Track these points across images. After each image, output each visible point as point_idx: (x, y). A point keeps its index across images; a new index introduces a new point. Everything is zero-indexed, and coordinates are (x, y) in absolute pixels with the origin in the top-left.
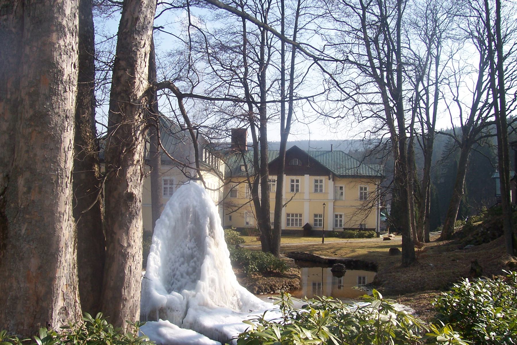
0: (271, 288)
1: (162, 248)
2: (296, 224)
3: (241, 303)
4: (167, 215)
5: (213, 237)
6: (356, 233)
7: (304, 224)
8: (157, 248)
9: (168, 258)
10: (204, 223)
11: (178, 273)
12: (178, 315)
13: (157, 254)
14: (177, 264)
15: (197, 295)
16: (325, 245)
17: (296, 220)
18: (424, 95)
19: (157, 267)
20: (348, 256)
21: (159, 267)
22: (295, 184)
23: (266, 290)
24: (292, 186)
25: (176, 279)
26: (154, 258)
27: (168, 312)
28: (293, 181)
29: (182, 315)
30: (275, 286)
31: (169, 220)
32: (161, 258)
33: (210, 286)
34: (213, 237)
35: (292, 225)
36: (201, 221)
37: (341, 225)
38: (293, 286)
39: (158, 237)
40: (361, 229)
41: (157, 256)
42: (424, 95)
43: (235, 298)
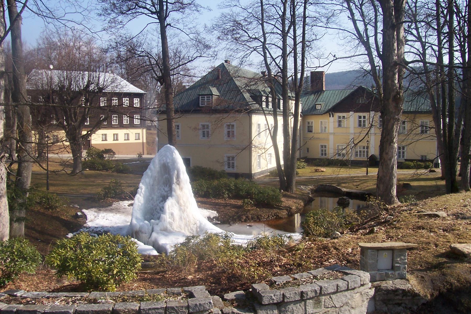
0: (258, 218)
1: (145, 191)
2: (364, 155)
3: (198, 230)
4: (150, 169)
5: (179, 184)
6: (412, 164)
7: (370, 155)
8: (141, 192)
9: (151, 198)
10: (173, 175)
11: (158, 208)
12: (144, 236)
13: (140, 196)
14: (158, 202)
15: (159, 224)
16: (368, 177)
17: (364, 152)
18: (445, 48)
19: (140, 204)
20: (370, 187)
21: (142, 204)
22: (362, 119)
23: (252, 218)
24: (360, 122)
25: (157, 212)
26: (138, 198)
27: (140, 234)
28: (360, 117)
29: (148, 237)
30: (261, 216)
31: (151, 172)
32: (144, 197)
33: (169, 218)
34: (179, 184)
35: (360, 155)
36: (171, 173)
37: (403, 157)
38: (278, 216)
39: (143, 184)
40: (421, 161)
41: (140, 197)
42: (445, 48)
43: (195, 226)
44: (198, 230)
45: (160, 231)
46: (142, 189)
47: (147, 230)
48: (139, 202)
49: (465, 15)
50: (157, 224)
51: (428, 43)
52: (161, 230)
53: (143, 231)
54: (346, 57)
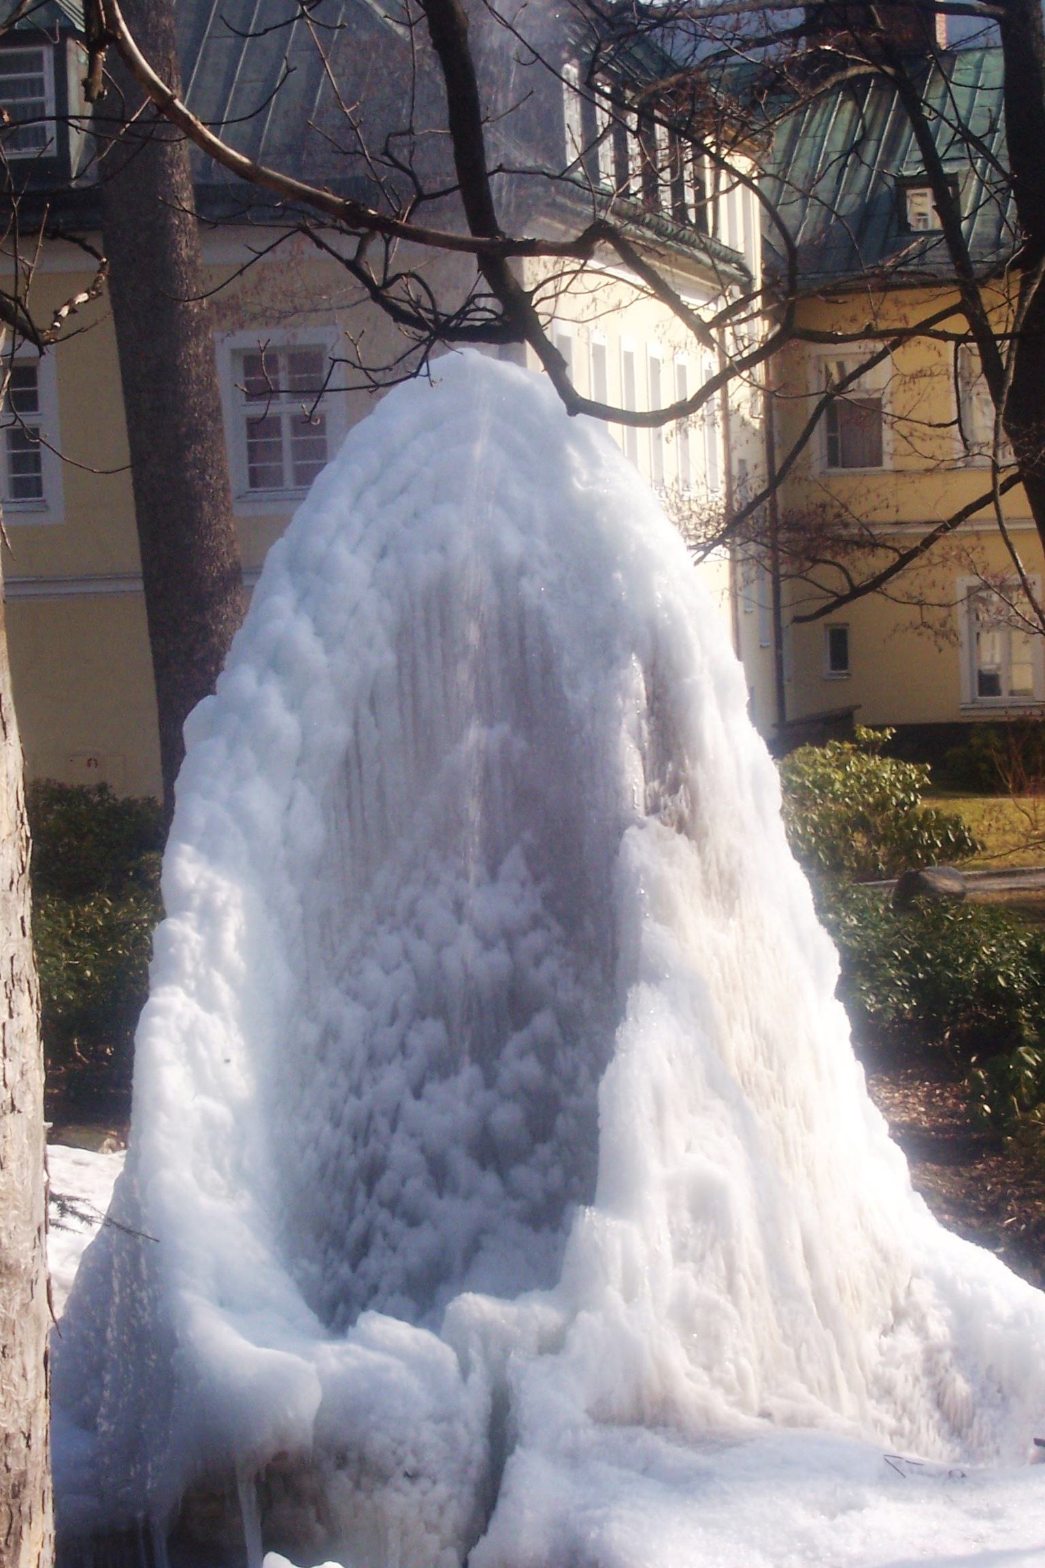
4: (278, 662)
9: (311, 1033)
10: (602, 710)
11: (402, 1151)
13: (208, 1002)
14: (393, 1078)
15: (577, 1341)
19: (221, 1111)
25: (393, 1205)
27: (342, 1482)
29: (456, 1516)
31: (294, 703)
33: (681, 1252)
36: (579, 697)
39: (212, 853)
43: (908, 1341)
44: (961, 1387)
45: (590, 1435)
46: (210, 917)
47: (429, 1434)
48: (201, 1086)
49: (696, 159)
50: (553, 1345)
51: (788, 183)
52: (603, 1416)
53: (379, 1442)
54: (387, 260)
